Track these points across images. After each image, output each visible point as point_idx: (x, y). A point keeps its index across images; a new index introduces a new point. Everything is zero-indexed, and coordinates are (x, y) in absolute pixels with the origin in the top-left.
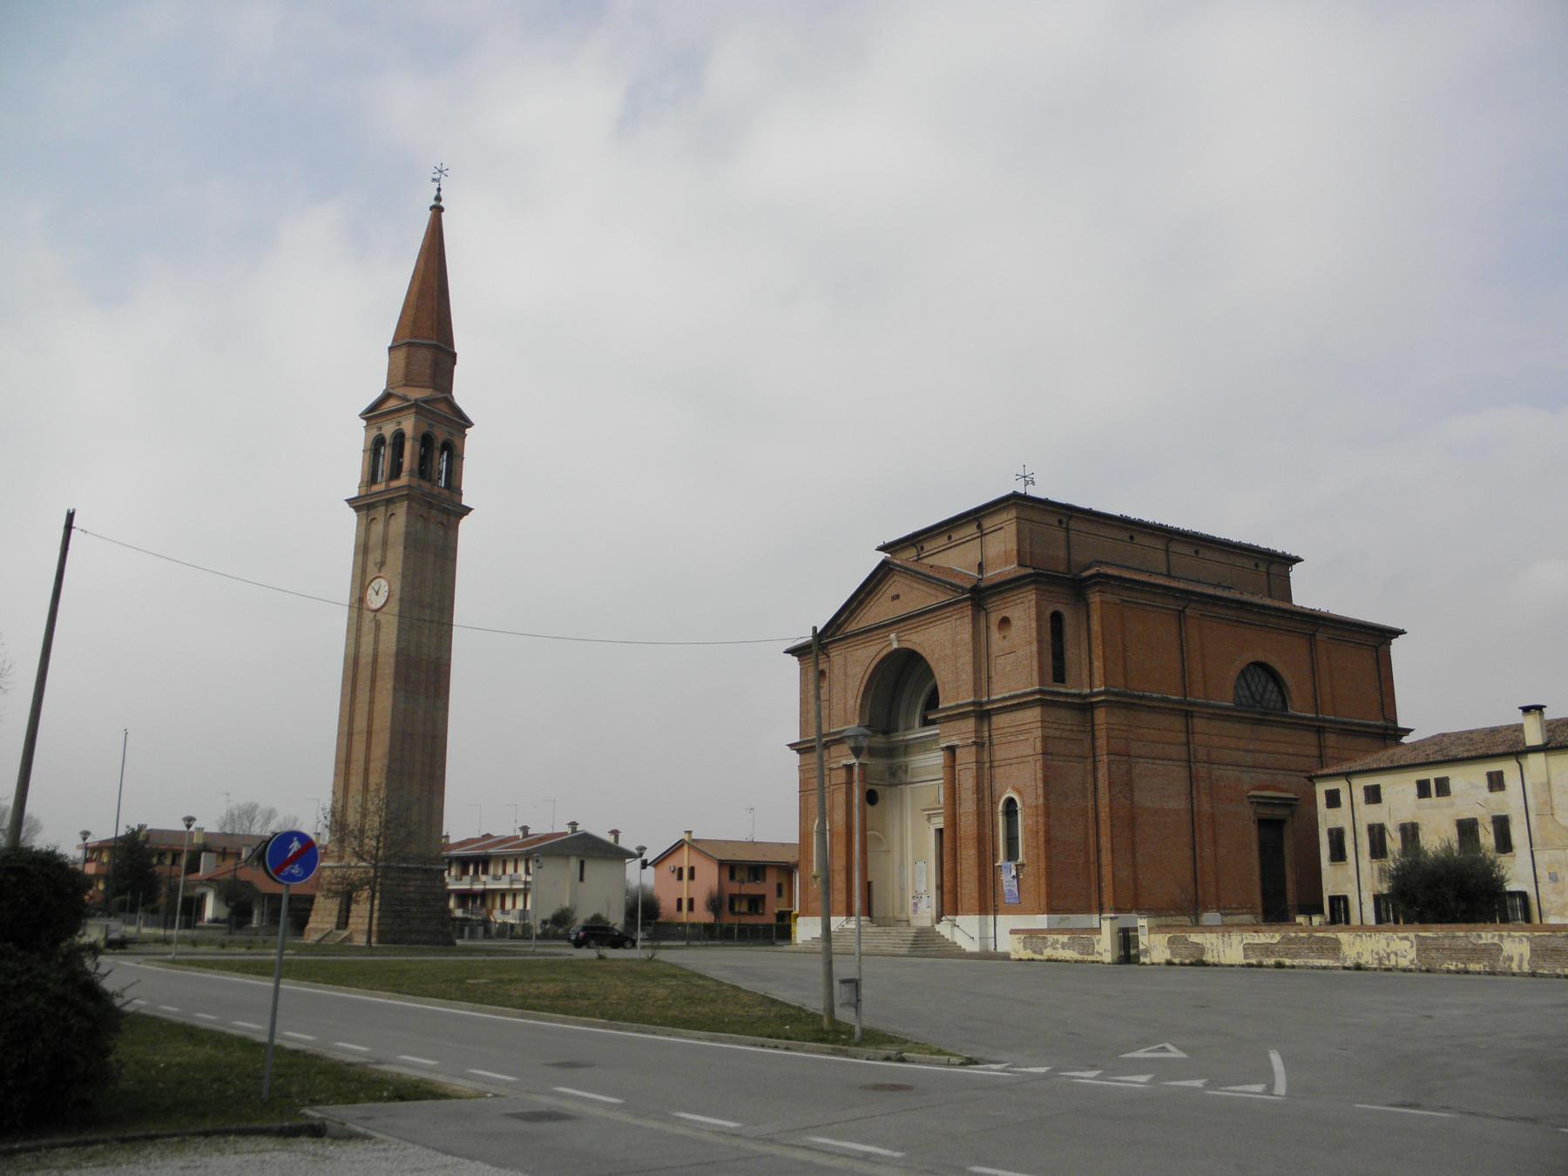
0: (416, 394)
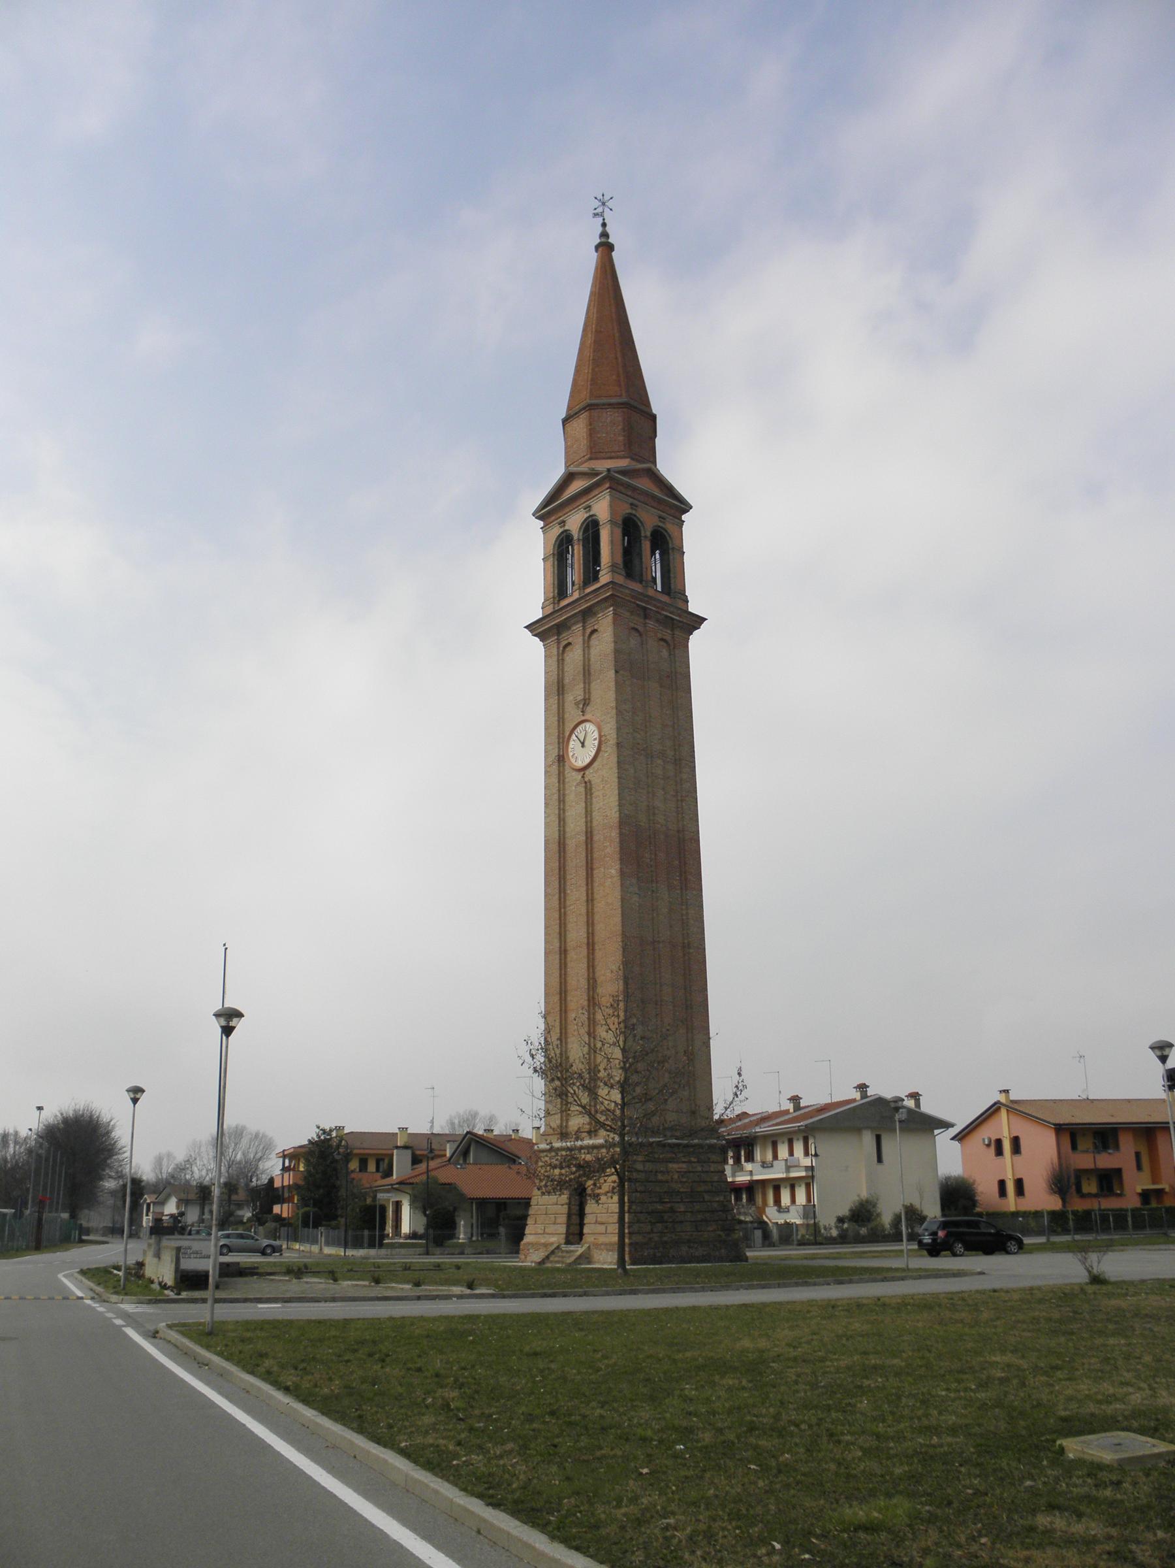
0: (603, 466)
